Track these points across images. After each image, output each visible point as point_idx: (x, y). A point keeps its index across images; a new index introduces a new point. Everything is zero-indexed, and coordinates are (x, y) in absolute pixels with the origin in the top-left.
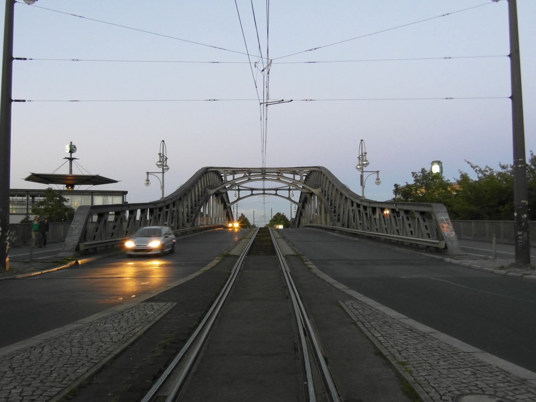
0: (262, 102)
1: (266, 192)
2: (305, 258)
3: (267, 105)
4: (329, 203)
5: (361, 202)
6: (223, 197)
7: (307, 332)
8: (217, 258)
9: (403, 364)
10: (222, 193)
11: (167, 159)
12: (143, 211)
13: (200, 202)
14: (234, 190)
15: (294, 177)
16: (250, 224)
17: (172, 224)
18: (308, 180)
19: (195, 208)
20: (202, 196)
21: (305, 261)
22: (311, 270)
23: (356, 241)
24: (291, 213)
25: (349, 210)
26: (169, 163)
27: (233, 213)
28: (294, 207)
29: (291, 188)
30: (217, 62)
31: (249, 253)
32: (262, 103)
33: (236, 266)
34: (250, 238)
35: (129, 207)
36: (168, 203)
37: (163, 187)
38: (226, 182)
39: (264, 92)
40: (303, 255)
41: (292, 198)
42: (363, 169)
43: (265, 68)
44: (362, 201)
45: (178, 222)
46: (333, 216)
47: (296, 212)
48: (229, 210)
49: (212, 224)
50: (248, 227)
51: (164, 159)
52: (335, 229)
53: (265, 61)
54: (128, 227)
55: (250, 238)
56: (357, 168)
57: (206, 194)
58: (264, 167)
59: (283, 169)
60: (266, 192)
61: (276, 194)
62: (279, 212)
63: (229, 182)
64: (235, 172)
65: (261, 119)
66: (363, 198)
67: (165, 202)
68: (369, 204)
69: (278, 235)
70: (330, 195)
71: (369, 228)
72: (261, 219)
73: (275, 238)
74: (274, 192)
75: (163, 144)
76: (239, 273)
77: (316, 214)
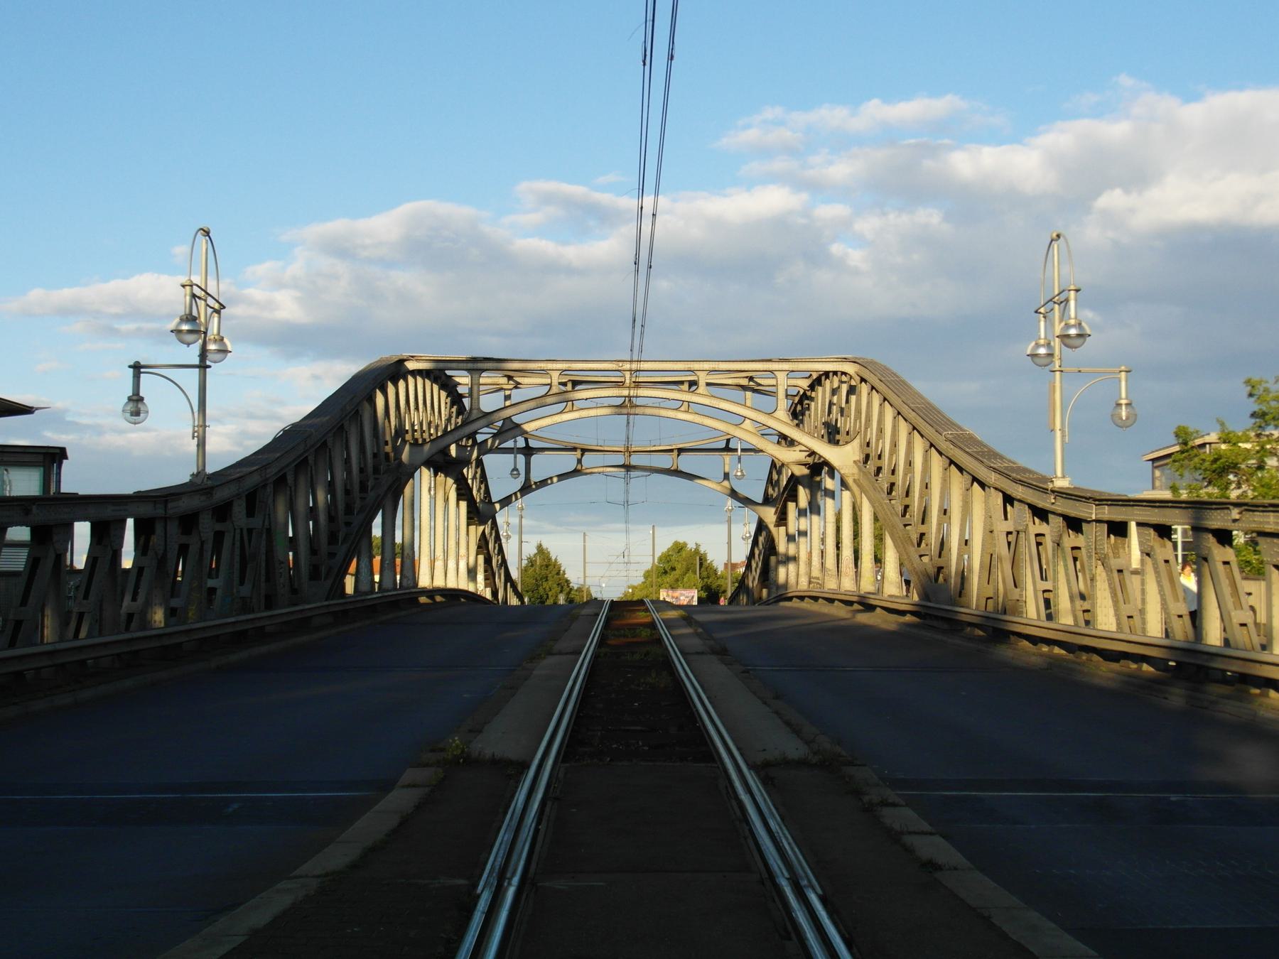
8: (410, 775)
12: (105, 537)
13: (371, 495)
24: (729, 543)
33: (503, 837)
35: (27, 512)
36: (221, 495)
38: (475, 415)
45: (268, 580)
54: (24, 602)
62: (681, 541)
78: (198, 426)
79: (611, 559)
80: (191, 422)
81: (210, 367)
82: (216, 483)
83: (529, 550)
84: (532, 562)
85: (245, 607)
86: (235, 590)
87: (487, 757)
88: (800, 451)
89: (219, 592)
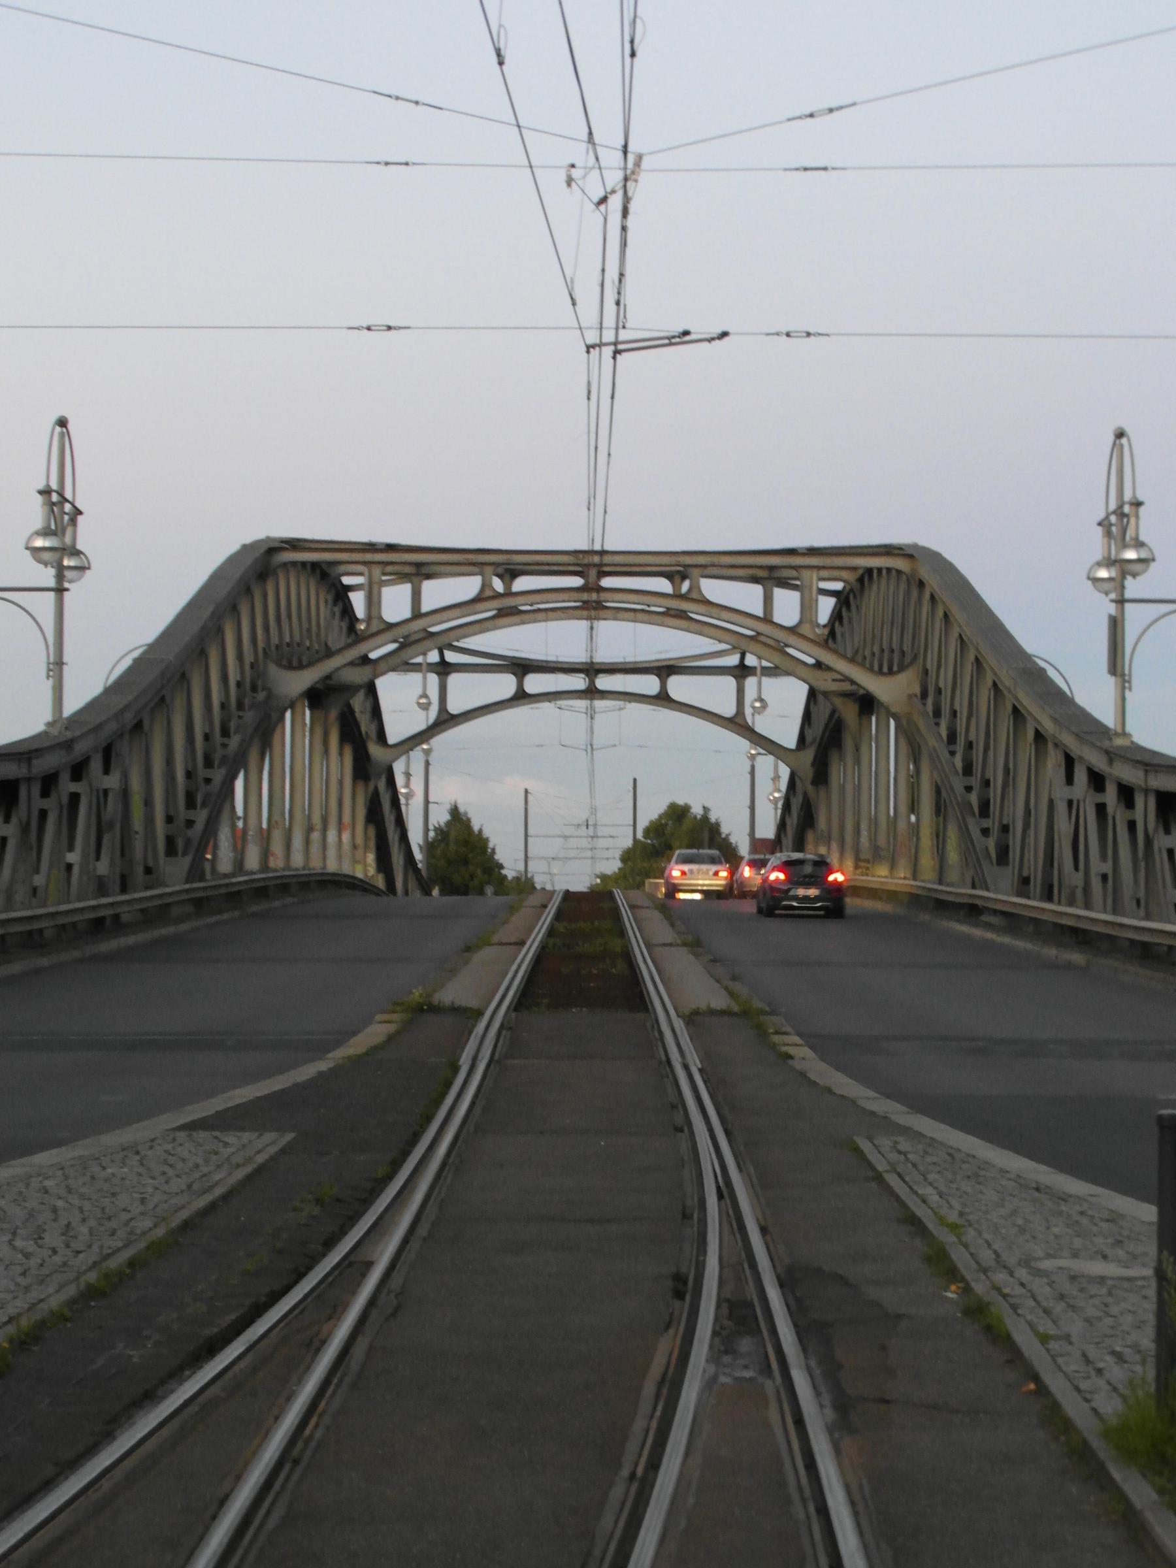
0: (592, 338)
1: (604, 682)
2: (771, 1022)
3: (617, 352)
4: (958, 762)
5: (1111, 761)
6: (351, 711)
7: (725, 1192)
8: (379, 1017)
9: (954, 1228)
10: (349, 689)
11: (80, 518)
13: (235, 741)
14: (417, 668)
15: (768, 600)
16: (504, 872)
17: (98, 864)
18: (850, 620)
19: (209, 773)
20: (240, 706)
21: (772, 1033)
22: (790, 1062)
23: (1069, 966)
24: (752, 808)
25: (1051, 803)
26: (86, 536)
27: (402, 800)
28: (772, 776)
29: (751, 660)
30: (403, 161)
31: (525, 1000)
32: (593, 346)
34: (515, 944)
36: (80, 748)
37: (57, 667)
38: (375, 626)
39: (603, 270)
40: (773, 1013)
41: (762, 725)
42: (1123, 587)
43: (613, 192)
44: (1111, 756)
46: (976, 833)
47: (780, 805)
48: (382, 785)
49: (239, 865)
50: (489, 890)
51: (66, 518)
52: (979, 902)
53: (612, 158)
55: (515, 944)
56: (1096, 581)
57: (261, 696)
58: (597, 547)
59: (701, 560)
60: (603, 682)
61: (663, 698)
62: (681, 802)
63: (390, 626)
64: (425, 570)
65: (589, 392)
66: (1119, 742)
67: (68, 745)
68: (1141, 774)
69: (662, 931)
70: (963, 713)
71: (1143, 903)
72: (573, 842)
73: (648, 945)
74: (649, 684)
75: (62, 435)
76: (492, 1066)
77: (913, 818)
78: (53, 664)
79: (569, 831)
80: (45, 659)
81: (67, 590)
82: (78, 733)
83: (440, 817)
84: (442, 833)
85: (102, 888)
86: (91, 867)
87: (447, 1005)
88: (834, 680)
89: (76, 870)
